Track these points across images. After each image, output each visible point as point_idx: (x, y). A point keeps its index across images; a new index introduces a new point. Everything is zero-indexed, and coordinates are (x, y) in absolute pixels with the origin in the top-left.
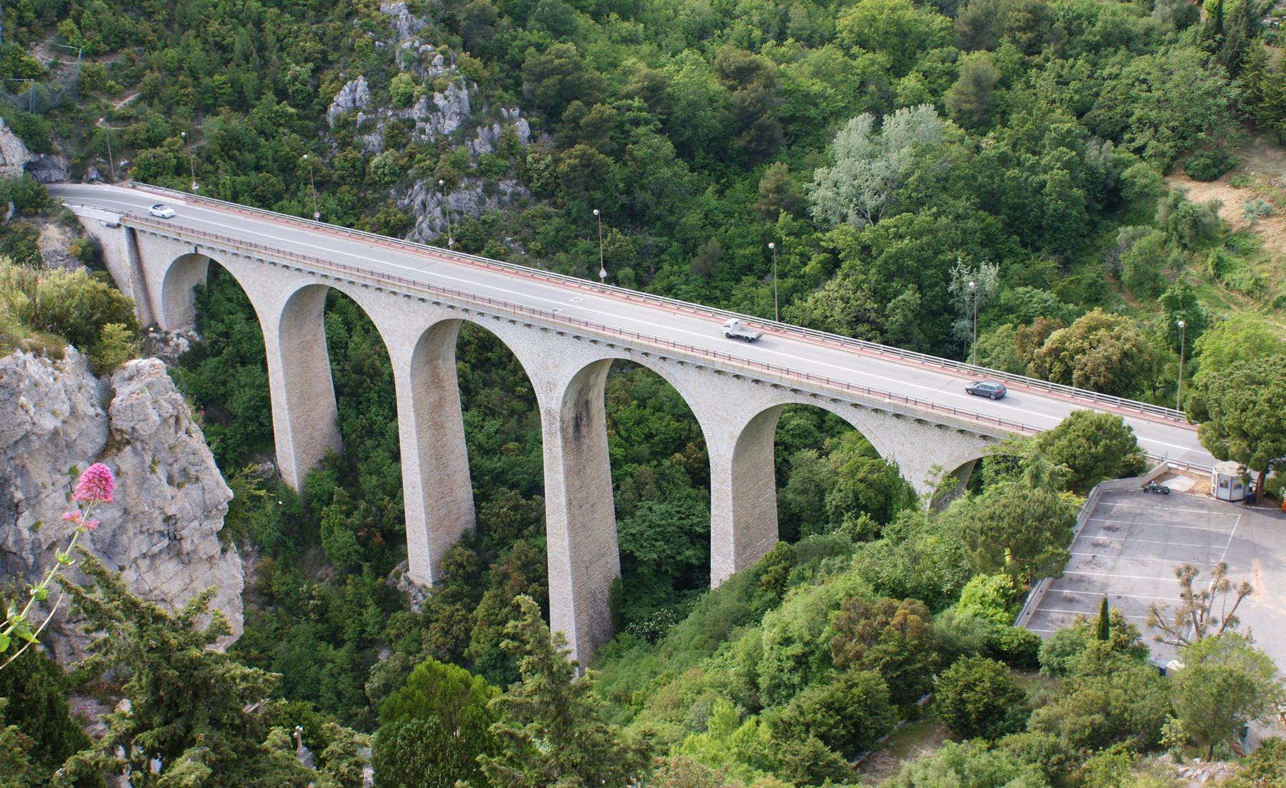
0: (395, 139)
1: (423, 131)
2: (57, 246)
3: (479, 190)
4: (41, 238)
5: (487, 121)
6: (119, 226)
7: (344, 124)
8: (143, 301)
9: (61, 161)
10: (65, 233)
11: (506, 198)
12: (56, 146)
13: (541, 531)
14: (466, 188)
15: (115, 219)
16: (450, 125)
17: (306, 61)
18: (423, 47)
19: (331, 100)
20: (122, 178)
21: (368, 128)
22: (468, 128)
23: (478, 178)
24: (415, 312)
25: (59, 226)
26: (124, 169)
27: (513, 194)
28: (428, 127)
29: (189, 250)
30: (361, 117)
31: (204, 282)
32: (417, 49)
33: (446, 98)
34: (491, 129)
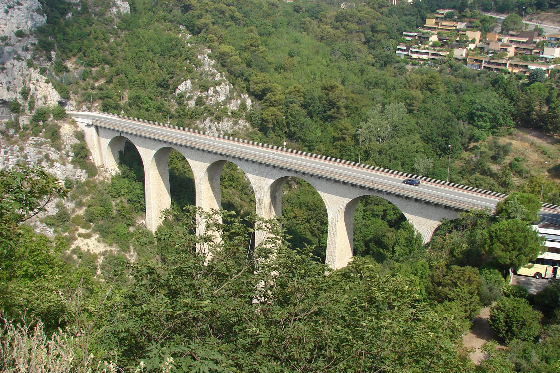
0: (200, 102)
1: (211, 100)
2: (68, 132)
3: (231, 123)
4: (62, 129)
5: (236, 97)
6: (92, 125)
7: (181, 96)
8: (99, 155)
9: (74, 103)
10: (71, 127)
11: (241, 127)
12: (72, 96)
13: (327, 155)
14: (227, 121)
15: (90, 122)
16: (222, 98)
17: (169, 74)
18: (213, 71)
19: (177, 88)
20: (96, 111)
21: (190, 98)
22: (229, 99)
23: (231, 118)
24: (206, 158)
25: (69, 124)
26: (97, 107)
27: (244, 126)
28: (213, 99)
29: (118, 134)
30: (188, 94)
31: (123, 150)
32: (211, 71)
33: (221, 88)
34: (237, 101)
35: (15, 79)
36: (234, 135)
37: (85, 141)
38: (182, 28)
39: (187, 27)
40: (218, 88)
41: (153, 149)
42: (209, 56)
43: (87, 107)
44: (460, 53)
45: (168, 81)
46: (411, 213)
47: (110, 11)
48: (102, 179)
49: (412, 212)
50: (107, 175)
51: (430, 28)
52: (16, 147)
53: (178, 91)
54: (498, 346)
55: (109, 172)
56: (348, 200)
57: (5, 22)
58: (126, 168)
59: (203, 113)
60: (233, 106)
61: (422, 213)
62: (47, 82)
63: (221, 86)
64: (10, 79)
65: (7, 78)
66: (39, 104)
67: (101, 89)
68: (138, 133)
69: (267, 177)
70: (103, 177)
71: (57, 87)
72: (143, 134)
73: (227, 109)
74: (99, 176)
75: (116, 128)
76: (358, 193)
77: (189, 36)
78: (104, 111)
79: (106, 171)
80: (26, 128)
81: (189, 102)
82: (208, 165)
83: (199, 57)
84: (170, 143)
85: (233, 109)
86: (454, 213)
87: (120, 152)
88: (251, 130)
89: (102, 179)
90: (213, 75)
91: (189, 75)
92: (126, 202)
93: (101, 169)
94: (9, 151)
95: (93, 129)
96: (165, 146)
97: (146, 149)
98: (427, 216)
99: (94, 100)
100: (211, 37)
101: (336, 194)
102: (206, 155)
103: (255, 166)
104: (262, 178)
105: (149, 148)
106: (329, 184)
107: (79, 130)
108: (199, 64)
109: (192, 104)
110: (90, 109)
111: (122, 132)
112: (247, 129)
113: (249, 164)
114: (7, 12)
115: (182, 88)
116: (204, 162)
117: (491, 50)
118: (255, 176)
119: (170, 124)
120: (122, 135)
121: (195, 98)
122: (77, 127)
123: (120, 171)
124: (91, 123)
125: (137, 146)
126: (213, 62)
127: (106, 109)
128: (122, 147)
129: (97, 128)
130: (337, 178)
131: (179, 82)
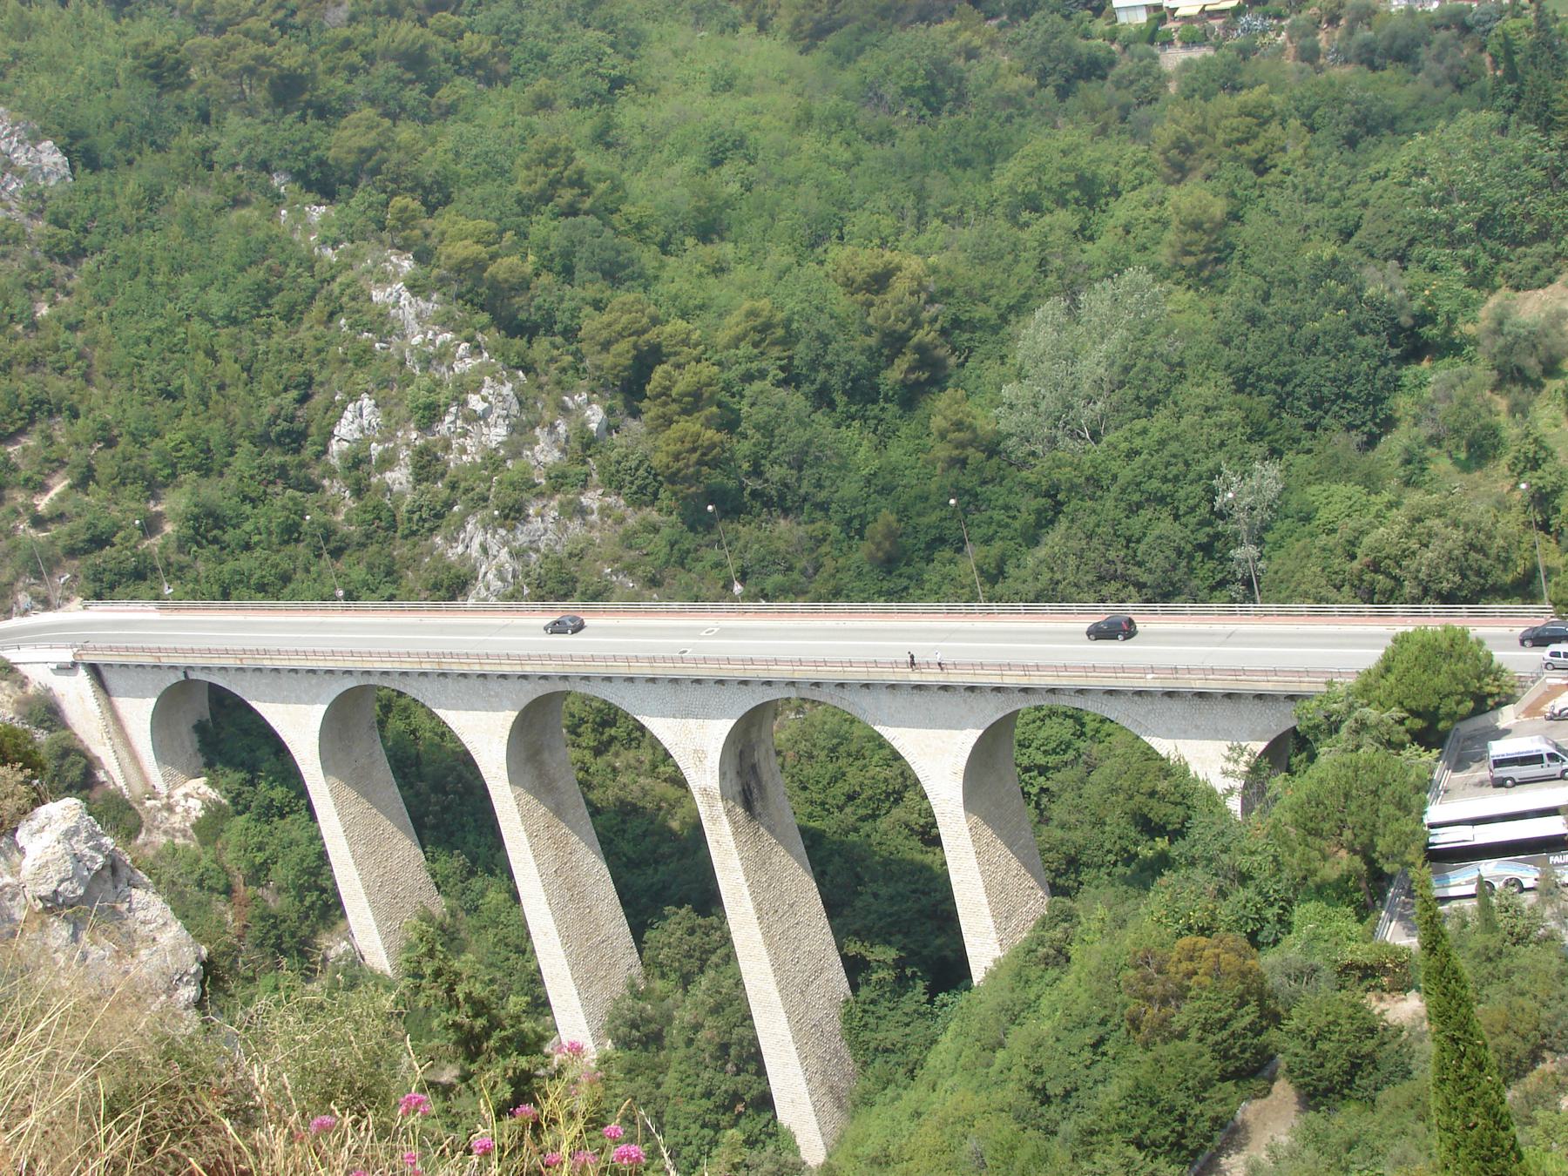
0: (427, 465)
1: (463, 450)
6: (74, 665)
7: (356, 461)
15: (67, 656)
16: (497, 433)
17: (286, 390)
21: (387, 462)
22: (521, 432)
24: (497, 695)
27: (602, 510)
29: (174, 678)
30: (376, 449)
31: (207, 715)
32: (432, 342)
37: (66, 727)
38: (279, 181)
39: (300, 177)
41: (313, 701)
42: (415, 288)
43: (35, 597)
45: (291, 419)
46: (1169, 734)
48: (164, 840)
49: (1170, 730)
50: (176, 820)
53: (335, 446)
54: (1431, 1080)
55: (179, 809)
56: (971, 736)
58: (235, 777)
59: (449, 505)
60: (545, 453)
61: (1197, 727)
63: (484, 392)
67: (60, 517)
68: (248, 663)
69: (707, 717)
70: (166, 832)
72: (267, 663)
73: (526, 471)
74: (149, 831)
76: (993, 711)
77: (317, 213)
78: (99, 596)
79: (170, 808)
81: (389, 476)
82: (512, 715)
83: (378, 296)
85: (549, 459)
86: (1290, 708)
87: (200, 728)
88: (633, 520)
89: (164, 840)
90: (444, 355)
91: (360, 376)
93: (149, 804)
95: (82, 678)
96: (350, 683)
97: (292, 707)
98: (1217, 731)
99: (53, 564)
100: (405, 209)
101: (932, 723)
102: (494, 686)
103: (658, 689)
104: (691, 722)
105: (299, 701)
106: (900, 700)
107: (30, 690)
108: (382, 323)
109: (399, 477)
110: (46, 604)
112: (621, 521)
113: (640, 687)
115: (346, 429)
116: (495, 710)
118: (671, 720)
120: (193, 676)
121: (404, 454)
122: (23, 682)
123: (214, 794)
124: (70, 659)
125: (254, 704)
126: (431, 307)
127: (103, 588)
128: (201, 708)
129: (95, 670)
131: (334, 411)
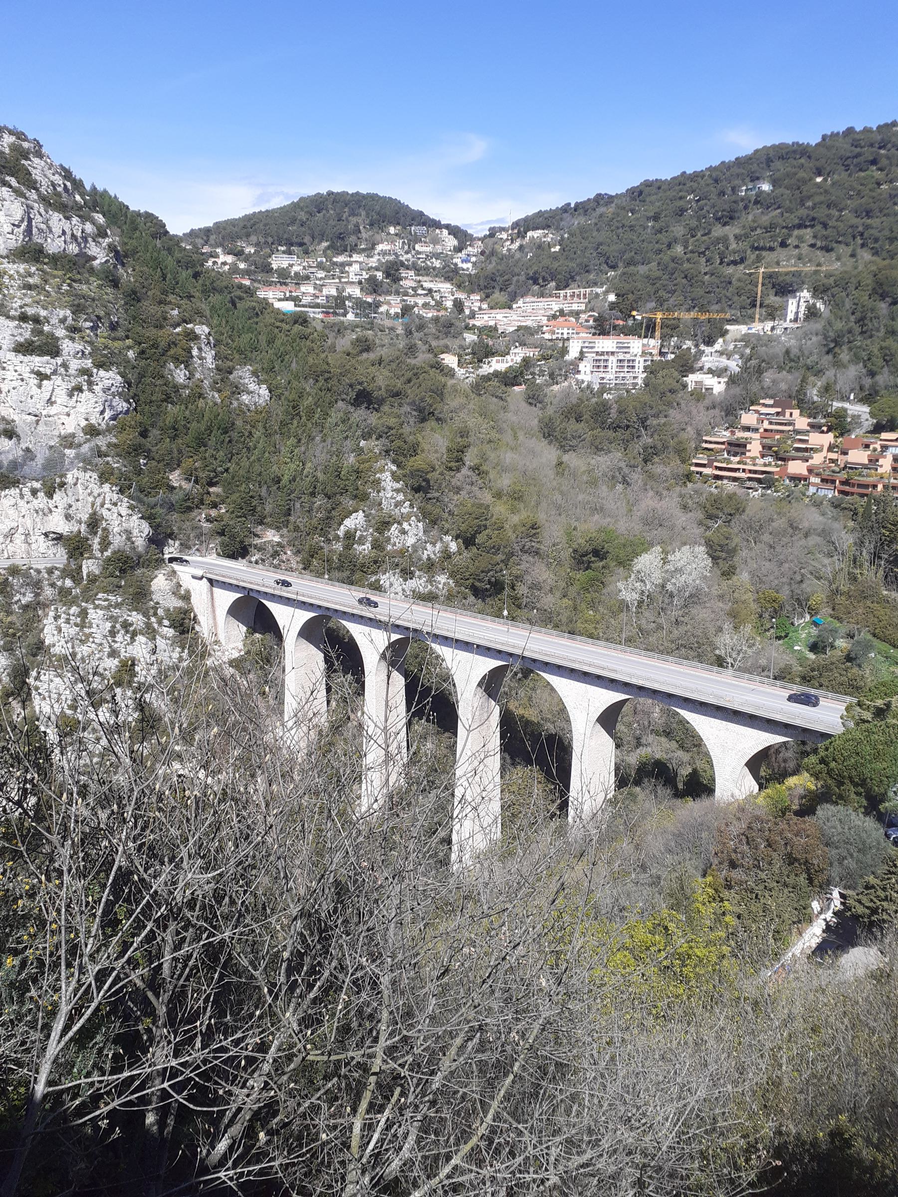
15: (199, 573)
35: (78, 500)
36: (429, 598)
40: (405, 526)
44: (797, 467)
47: (238, 399)
51: (747, 429)
52: (74, 610)
57: (67, 410)
62: (131, 507)
64: (71, 500)
65: (65, 499)
66: (117, 541)
71: (107, 214)
75: (242, 584)
80: (92, 579)
84: (328, 609)
92: (470, 424)
94: (63, 615)
111: (252, 590)
114: (71, 395)
117: (850, 463)
119: (329, 579)
120: (251, 594)
129: (211, 581)
130: (586, 669)
